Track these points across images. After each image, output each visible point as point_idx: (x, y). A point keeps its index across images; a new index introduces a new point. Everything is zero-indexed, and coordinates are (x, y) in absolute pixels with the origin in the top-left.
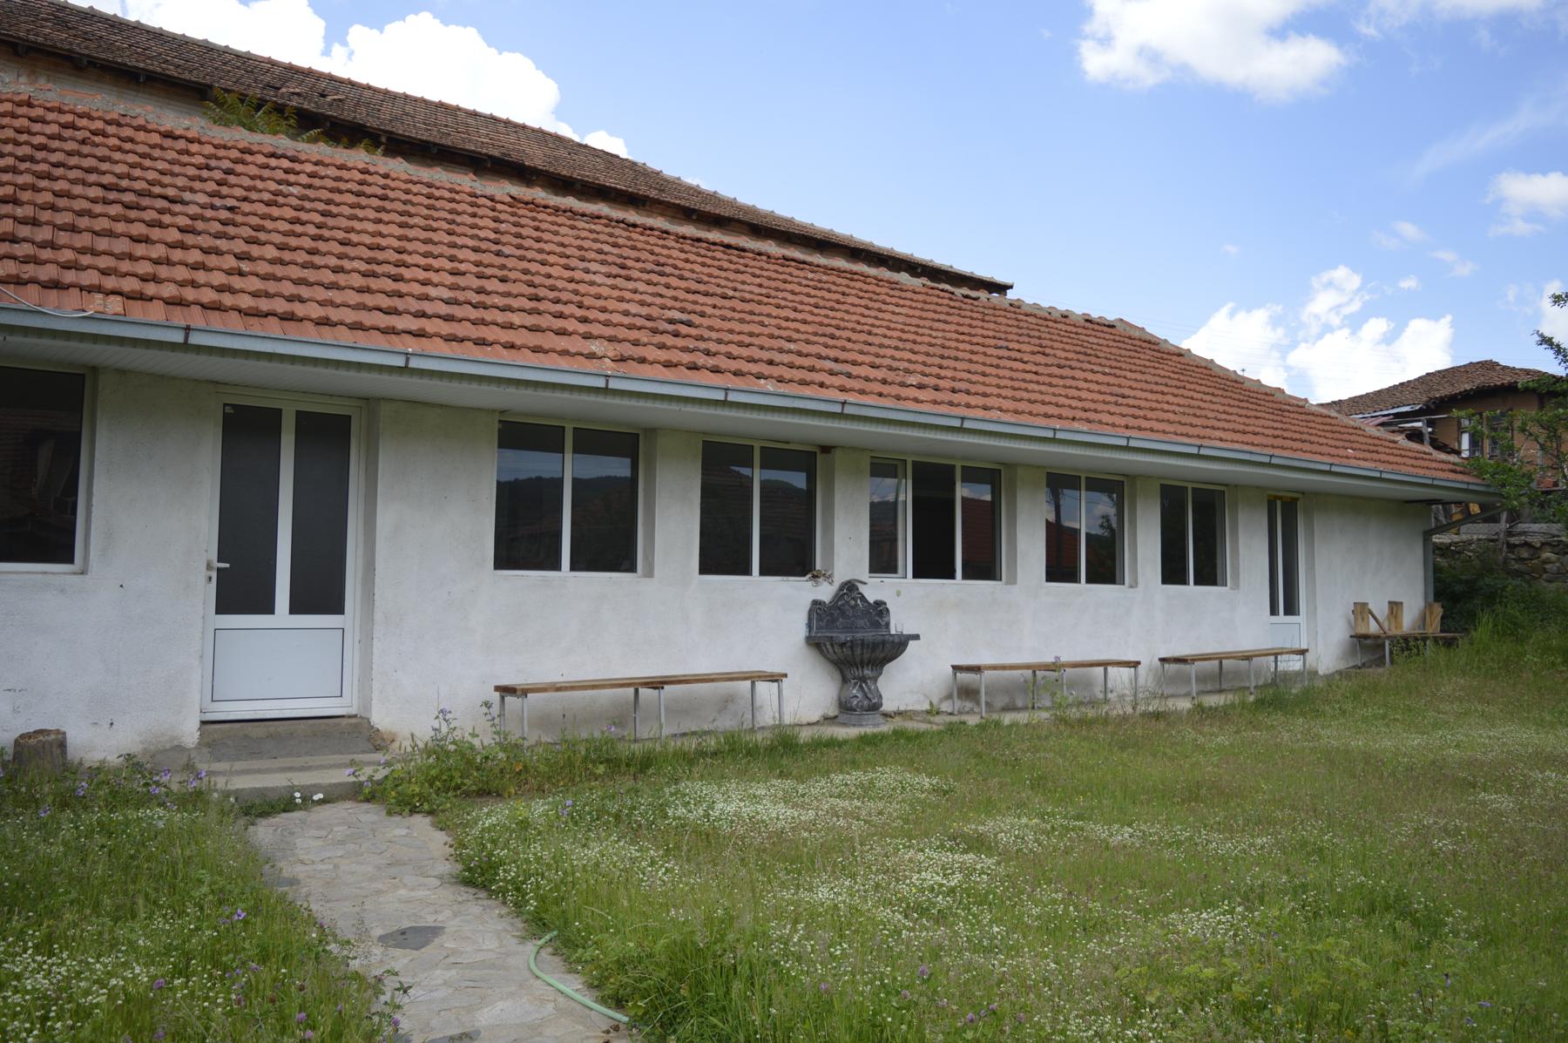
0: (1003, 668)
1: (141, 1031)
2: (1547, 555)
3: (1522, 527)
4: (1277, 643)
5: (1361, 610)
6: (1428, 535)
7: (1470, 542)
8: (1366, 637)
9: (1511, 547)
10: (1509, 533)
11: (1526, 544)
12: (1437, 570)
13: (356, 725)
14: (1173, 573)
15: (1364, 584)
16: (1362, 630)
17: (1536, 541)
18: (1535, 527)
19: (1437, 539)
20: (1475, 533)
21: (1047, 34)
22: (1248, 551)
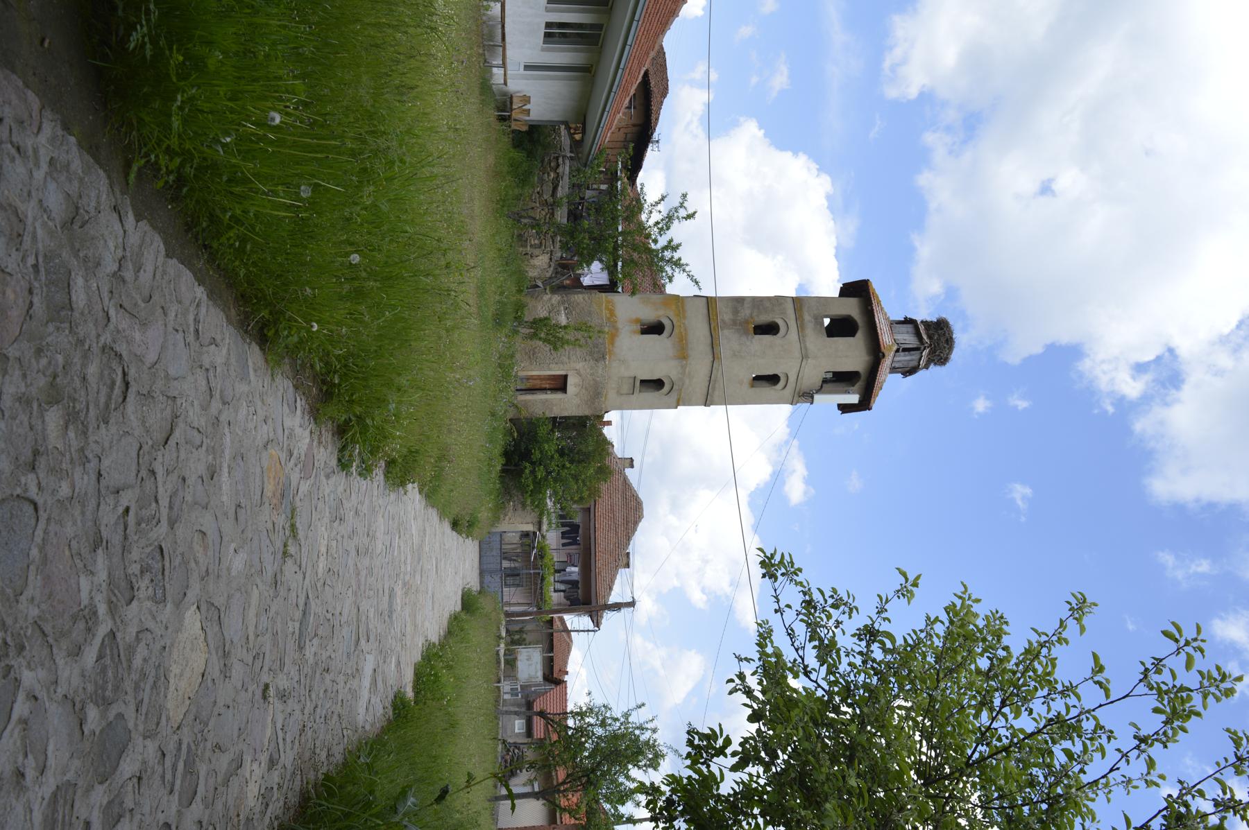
0: (503, 27)
1: (207, 370)
2: (552, 175)
3: (567, 162)
4: (509, 67)
5: (526, 99)
6: (566, 123)
7: (560, 136)
8: (511, 103)
9: (557, 158)
10: (564, 157)
11: (558, 166)
12: (546, 127)
13: (491, 36)
14: (549, 25)
15: (542, 98)
16: (515, 100)
17: (560, 170)
18: (567, 168)
19: (563, 127)
20: (565, 140)
21: (1020, 492)
22: (562, 56)
